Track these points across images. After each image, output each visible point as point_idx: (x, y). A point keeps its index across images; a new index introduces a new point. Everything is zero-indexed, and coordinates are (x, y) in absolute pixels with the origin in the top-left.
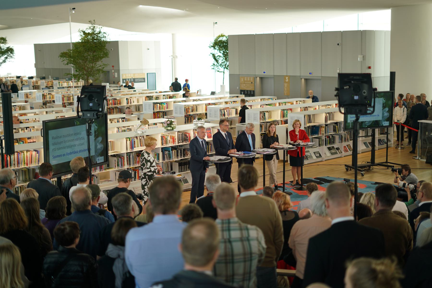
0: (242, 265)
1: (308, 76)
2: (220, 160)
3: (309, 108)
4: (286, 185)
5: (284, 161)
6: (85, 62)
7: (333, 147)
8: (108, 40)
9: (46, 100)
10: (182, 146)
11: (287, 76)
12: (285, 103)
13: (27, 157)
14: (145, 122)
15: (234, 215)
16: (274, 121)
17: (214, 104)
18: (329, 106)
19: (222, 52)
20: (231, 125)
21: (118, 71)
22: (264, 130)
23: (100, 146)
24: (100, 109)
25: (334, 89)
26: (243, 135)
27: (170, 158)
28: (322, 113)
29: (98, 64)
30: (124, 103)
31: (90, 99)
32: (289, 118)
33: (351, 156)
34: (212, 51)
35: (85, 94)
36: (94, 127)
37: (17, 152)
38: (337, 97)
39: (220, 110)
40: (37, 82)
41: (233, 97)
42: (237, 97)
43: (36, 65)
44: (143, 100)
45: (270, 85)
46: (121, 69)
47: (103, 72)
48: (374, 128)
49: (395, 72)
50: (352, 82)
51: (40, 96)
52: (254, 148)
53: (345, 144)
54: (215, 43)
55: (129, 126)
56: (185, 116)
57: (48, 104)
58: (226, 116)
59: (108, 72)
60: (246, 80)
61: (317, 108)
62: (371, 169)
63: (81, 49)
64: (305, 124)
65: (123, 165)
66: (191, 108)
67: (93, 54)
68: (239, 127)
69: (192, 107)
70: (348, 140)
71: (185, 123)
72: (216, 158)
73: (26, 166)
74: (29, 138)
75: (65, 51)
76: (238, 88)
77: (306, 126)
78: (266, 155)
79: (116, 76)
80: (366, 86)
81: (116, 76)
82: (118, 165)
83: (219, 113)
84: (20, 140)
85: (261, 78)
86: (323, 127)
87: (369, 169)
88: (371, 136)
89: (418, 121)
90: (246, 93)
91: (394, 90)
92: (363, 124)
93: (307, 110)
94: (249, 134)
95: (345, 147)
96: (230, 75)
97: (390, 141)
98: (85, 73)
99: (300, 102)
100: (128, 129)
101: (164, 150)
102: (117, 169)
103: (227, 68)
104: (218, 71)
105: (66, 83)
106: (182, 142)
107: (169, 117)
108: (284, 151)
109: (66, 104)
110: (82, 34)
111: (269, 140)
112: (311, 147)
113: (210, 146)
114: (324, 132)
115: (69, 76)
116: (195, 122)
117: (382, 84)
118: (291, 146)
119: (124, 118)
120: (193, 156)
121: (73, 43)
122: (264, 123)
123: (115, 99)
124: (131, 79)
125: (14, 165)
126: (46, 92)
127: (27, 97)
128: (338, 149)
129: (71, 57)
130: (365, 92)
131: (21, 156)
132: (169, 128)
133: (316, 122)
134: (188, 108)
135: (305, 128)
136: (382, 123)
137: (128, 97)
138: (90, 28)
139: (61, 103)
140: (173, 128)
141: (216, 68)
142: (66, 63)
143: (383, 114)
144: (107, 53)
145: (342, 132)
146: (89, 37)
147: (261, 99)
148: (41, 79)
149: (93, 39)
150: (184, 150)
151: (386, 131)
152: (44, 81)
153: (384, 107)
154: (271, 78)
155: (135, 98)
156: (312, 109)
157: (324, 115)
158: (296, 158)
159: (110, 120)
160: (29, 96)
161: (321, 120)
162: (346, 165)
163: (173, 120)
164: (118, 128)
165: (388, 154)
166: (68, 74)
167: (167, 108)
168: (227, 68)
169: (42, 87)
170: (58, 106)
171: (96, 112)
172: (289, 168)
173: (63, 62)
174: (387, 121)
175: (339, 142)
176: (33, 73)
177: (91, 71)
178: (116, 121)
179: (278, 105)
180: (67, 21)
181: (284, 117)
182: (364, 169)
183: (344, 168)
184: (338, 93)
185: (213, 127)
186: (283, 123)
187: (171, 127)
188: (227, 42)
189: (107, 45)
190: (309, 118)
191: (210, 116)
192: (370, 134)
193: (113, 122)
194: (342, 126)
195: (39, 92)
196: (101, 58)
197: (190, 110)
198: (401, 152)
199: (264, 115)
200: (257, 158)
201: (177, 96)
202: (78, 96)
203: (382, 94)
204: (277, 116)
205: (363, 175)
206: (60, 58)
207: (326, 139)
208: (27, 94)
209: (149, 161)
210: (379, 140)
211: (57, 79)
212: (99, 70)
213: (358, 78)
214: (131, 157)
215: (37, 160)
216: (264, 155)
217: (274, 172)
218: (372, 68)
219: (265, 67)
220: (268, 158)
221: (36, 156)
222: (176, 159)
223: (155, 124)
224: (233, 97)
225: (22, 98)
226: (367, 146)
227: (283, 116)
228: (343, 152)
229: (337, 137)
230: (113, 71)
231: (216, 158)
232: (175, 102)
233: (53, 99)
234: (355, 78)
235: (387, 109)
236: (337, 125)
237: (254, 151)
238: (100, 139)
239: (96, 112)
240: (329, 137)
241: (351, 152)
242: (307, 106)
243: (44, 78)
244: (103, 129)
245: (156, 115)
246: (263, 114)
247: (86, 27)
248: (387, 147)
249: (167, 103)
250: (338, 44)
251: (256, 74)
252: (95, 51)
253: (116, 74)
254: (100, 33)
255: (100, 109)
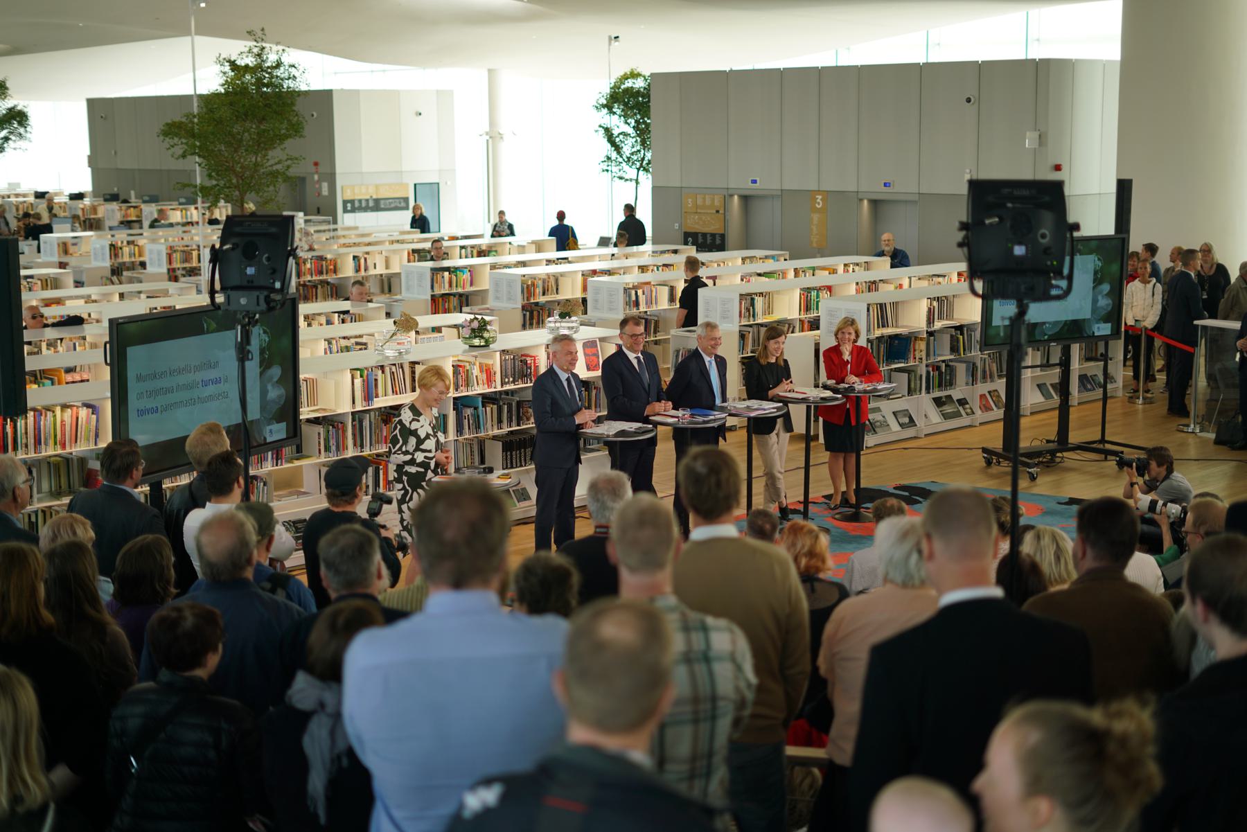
0: (687, 732)
1: (878, 191)
2: (622, 433)
3: (881, 285)
4: (810, 506)
5: (808, 438)
6: (236, 151)
7: (949, 397)
8: (304, 88)
9: (120, 260)
10: (513, 392)
11: (819, 192)
12: (814, 269)
13: (63, 425)
14: (406, 324)
15: (668, 588)
16: (780, 322)
17: (608, 272)
18: (941, 279)
19: (632, 121)
20: (655, 332)
21: (331, 178)
22: (750, 348)
23: (275, 393)
24: (278, 285)
25: (957, 224)
26: (691, 365)
27: (478, 427)
28: (919, 299)
29: (273, 157)
30: (348, 270)
31: (249, 254)
32: (822, 313)
33: (1001, 424)
34: (605, 118)
35: (235, 240)
36: (258, 337)
37: (34, 410)
38: (965, 249)
39: (625, 289)
40: (94, 209)
41: (663, 252)
42: (675, 252)
43: (92, 161)
44: (401, 260)
45: (767, 217)
46: (339, 170)
47: (287, 179)
48: (1067, 343)
49: (1130, 181)
50: (1009, 205)
51: (103, 248)
52: (724, 399)
53: (983, 388)
54: (611, 96)
55: (361, 336)
56: (524, 308)
57: (125, 273)
58: (643, 308)
59: (302, 180)
60: (699, 202)
61: (906, 285)
62: (1058, 460)
63: (225, 112)
64: (869, 330)
65: (341, 447)
66: (540, 283)
67: (258, 127)
68: (678, 339)
69: (544, 281)
70: (991, 376)
71: (524, 327)
72: (612, 428)
73: (60, 451)
74: (69, 370)
75: (177, 119)
76: (677, 226)
77: (872, 337)
78: (755, 418)
79: (325, 192)
80: (1048, 217)
81: (325, 192)
82: (327, 449)
83: (621, 297)
84: (42, 376)
85: (746, 199)
86: (922, 339)
87: (1052, 460)
88: (1060, 364)
89: (1196, 322)
90: (700, 240)
91: (1128, 232)
92: (1037, 331)
93: (877, 290)
94: (709, 355)
95: (982, 396)
96: (654, 188)
97: (1113, 380)
98: (234, 181)
99: (857, 268)
100: (357, 344)
101: (459, 403)
102: (323, 459)
103: (645, 169)
104: (621, 178)
105: (178, 213)
106: (514, 382)
107: (476, 309)
108: (808, 408)
109: (179, 273)
110: (227, 68)
111: (763, 376)
112: (886, 397)
113: (594, 392)
114: (924, 355)
115: (188, 191)
116: (552, 325)
117: (1093, 215)
118: (828, 394)
119: (347, 312)
120: (542, 420)
121: (201, 97)
122: (750, 326)
123: (321, 258)
124: (367, 200)
125: (26, 446)
126: (122, 236)
127: (66, 252)
128: (963, 402)
129: (193, 136)
130: (1045, 233)
131: (47, 421)
132: (476, 342)
133: (900, 323)
134: (533, 284)
135: (868, 341)
136: (1090, 327)
137: (359, 251)
138: (250, 51)
139: (165, 270)
140: (487, 341)
141: (615, 169)
142: (181, 152)
143: (1095, 301)
144: (299, 123)
145: (975, 354)
146: (248, 77)
147: (744, 259)
148: (106, 200)
149: (259, 83)
150: (519, 404)
151: (1101, 350)
152: (114, 206)
153: (1098, 281)
154: (773, 197)
155: (377, 256)
156: (891, 287)
157: (924, 305)
158: (843, 429)
159: (306, 317)
160: (71, 249)
161: (915, 319)
162: (985, 450)
163: (487, 318)
164: (329, 341)
165: (1107, 418)
166: (185, 186)
167: (471, 284)
168: (646, 170)
169: (108, 223)
170: (155, 278)
171: (266, 293)
172: (821, 455)
173: (170, 152)
174: (1106, 322)
175: (967, 384)
176: (83, 181)
177: (252, 177)
178: (323, 320)
179: (791, 274)
180: (185, 32)
181: (808, 309)
182: (1036, 461)
183: (979, 458)
184: (966, 237)
185: (602, 340)
186: (806, 326)
187: (482, 337)
188: (646, 93)
189: (299, 101)
190: (882, 313)
191: (596, 308)
192: (1055, 359)
193: (315, 324)
194: (977, 335)
195: (99, 237)
196: (283, 138)
197: (539, 290)
198: (1144, 411)
199: (753, 304)
200: (732, 429)
201: (499, 249)
202: (213, 246)
203: (1094, 244)
204: (788, 308)
205: (1033, 478)
206: (162, 138)
207: (928, 373)
208: (65, 244)
209: (414, 433)
210: (1083, 379)
211: (153, 199)
212: (274, 175)
213: (1025, 193)
214: (366, 423)
215: (93, 434)
216: (749, 419)
217: (779, 467)
218: (1065, 168)
219: (755, 166)
220: (760, 427)
221: (88, 421)
222: (496, 432)
223: (437, 330)
224: (663, 252)
225: (52, 255)
226: (1047, 395)
227: (807, 306)
228: (978, 412)
229: (961, 369)
230: (316, 177)
231: (612, 428)
232: (494, 267)
233: (142, 259)
234: (1017, 193)
235: (1106, 287)
236: (962, 334)
237: (722, 409)
238: (276, 372)
239: (266, 293)
240: (938, 368)
241: (1002, 411)
242: (877, 279)
243: (113, 198)
244: (286, 342)
245: (439, 304)
246: (748, 300)
247: (240, 50)
248: (1105, 399)
249: (471, 269)
250: (969, 100)
251: (731, 186)
252: (264, 119)
253: (325, 186)
254: (279, 65)
255: (278, 285)
